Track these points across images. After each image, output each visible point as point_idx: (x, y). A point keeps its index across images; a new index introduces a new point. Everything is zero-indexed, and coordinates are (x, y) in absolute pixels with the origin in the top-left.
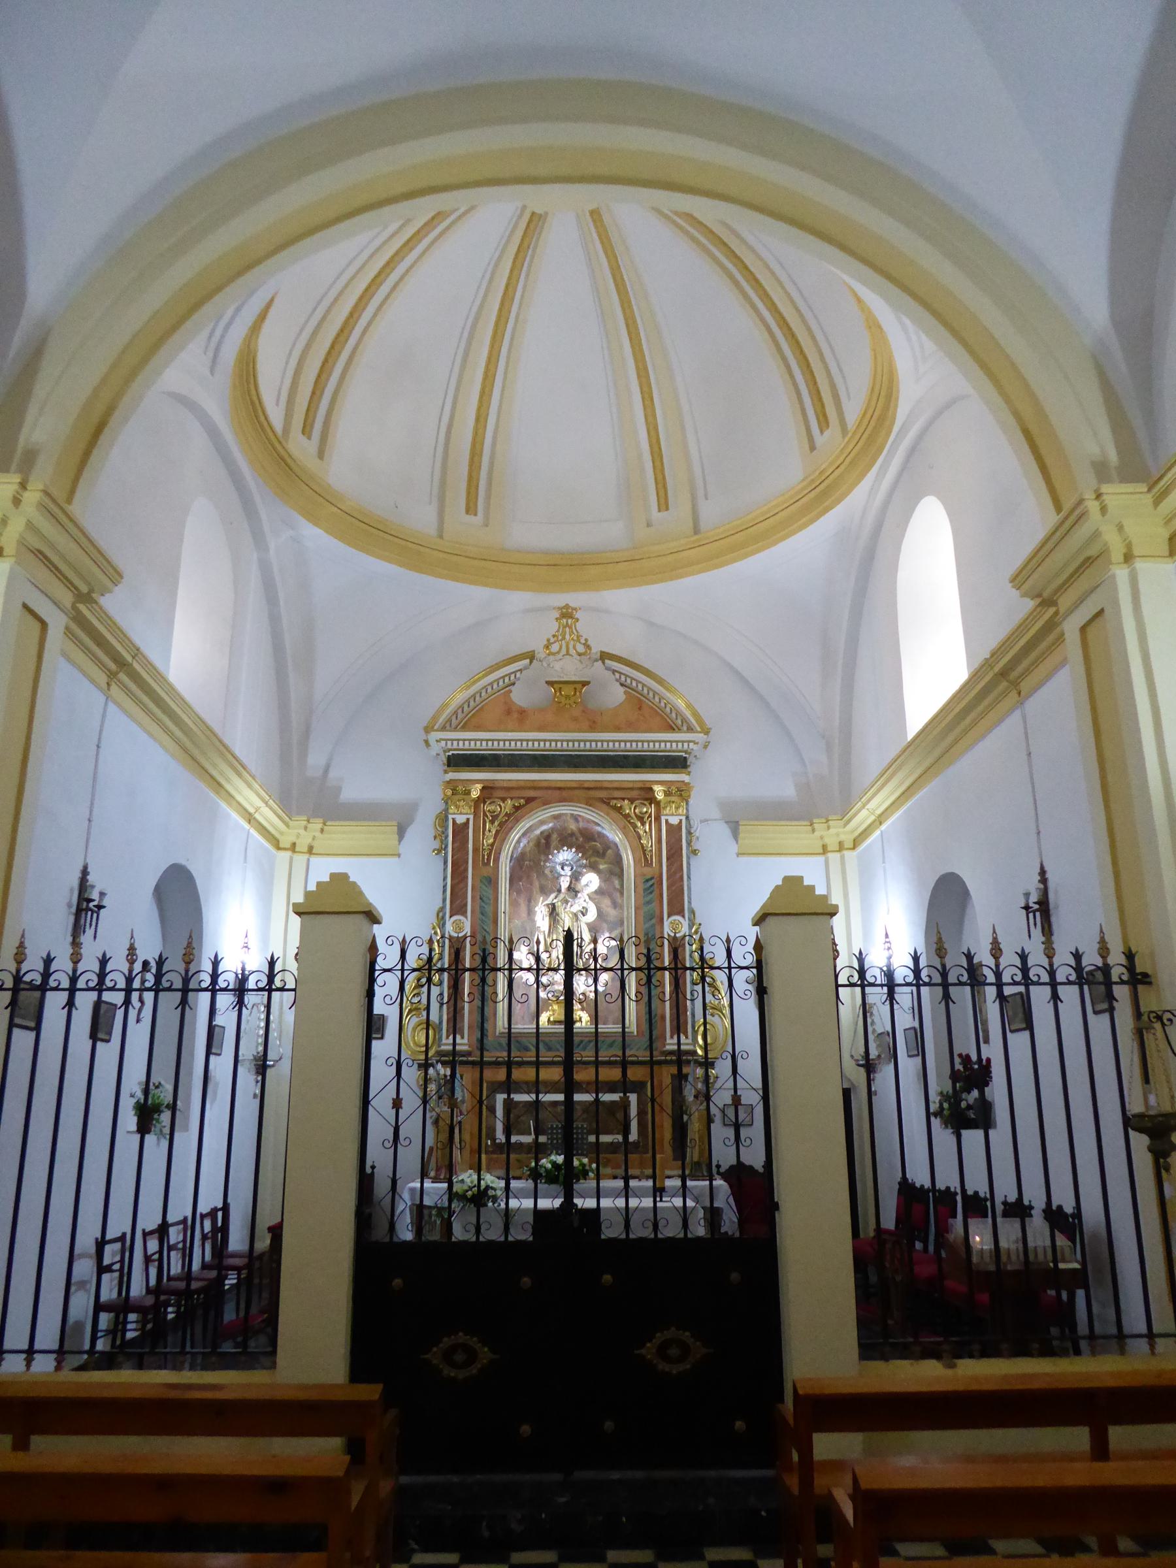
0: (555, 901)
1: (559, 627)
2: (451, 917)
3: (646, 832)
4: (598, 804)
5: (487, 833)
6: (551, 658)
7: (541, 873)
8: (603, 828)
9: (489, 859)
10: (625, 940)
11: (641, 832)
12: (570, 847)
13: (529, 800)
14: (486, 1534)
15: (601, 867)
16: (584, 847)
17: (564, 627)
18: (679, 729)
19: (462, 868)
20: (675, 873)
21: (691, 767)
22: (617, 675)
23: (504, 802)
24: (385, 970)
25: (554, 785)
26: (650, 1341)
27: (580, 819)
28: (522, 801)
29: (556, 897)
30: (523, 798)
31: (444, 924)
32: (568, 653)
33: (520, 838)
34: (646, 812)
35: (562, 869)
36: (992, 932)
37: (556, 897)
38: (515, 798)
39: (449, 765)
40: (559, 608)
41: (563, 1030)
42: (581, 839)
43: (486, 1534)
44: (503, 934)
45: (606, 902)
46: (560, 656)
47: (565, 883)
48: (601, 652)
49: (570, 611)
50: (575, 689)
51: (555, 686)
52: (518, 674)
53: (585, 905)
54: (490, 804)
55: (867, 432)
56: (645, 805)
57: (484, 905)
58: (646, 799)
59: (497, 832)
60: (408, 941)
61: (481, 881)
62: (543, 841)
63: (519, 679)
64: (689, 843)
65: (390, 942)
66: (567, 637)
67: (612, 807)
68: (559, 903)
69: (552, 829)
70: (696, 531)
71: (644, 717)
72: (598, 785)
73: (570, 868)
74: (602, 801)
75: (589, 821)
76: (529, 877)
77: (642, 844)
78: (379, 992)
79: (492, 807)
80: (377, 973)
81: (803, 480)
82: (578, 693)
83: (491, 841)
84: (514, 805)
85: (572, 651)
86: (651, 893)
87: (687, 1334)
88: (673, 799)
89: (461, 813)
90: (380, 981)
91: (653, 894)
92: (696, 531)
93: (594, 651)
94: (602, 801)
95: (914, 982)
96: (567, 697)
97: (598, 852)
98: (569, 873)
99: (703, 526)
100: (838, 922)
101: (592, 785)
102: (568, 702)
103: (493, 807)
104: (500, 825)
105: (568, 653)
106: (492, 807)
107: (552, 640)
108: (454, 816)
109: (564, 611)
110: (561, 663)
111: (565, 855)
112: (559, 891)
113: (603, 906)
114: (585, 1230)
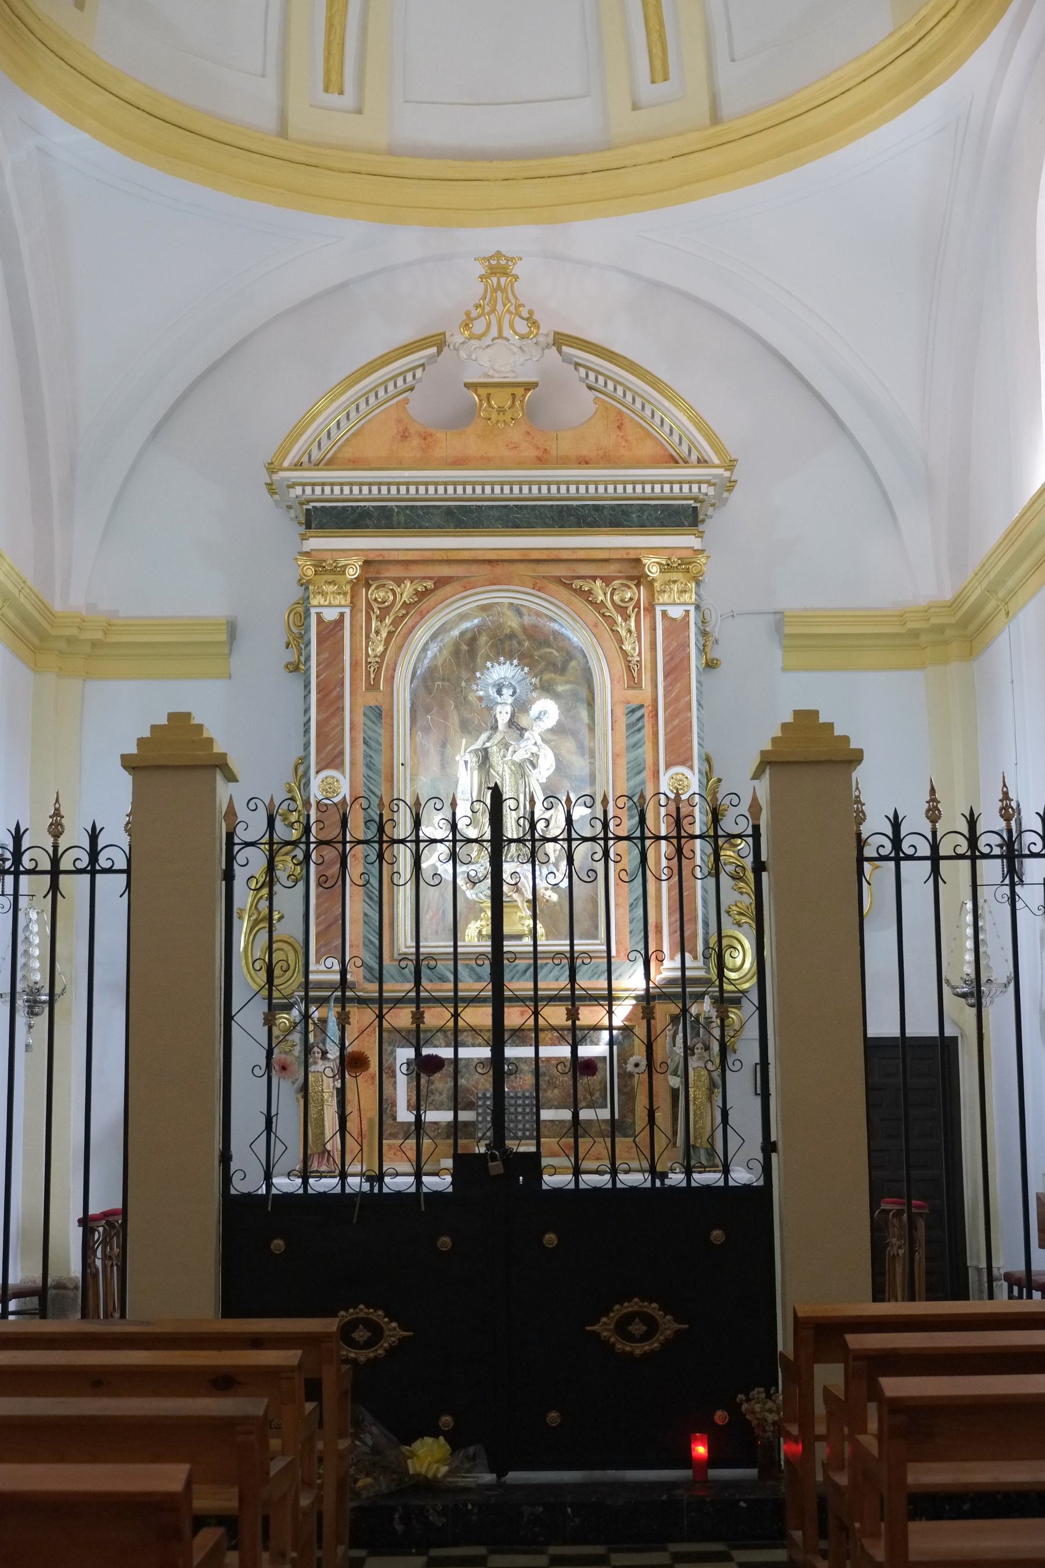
0: (488, 745)
1: (486, 291)
2: (317, 772)
3: (630, 631)
4: (554, 588)
5: (373, 635)
6: (474, 343)
7: (463, 701)
8: (562, 626)
9: (377, 679)
10: (574, 801)
11: (623, 633)
12: (510, 656)
13: (441, 582)
14: (399, 1527)
15: (560, 688)
16: (531, 657)
17: (495, 291)
18: (686, 462)
19: (334, 694)
20: (677, 699)
21: (708, 521)
22: (582, 372)
23: (399, 586)
24: (248, 844)
25: (482, 556)
26: (607, 1315)
27: (523, 610)
28: (430, 584)
29: (489, 739)
30: (431, 578)
31: (307, 784)
32: (500, 336)
33: (427, 643)
34: (631, 599)
35: (499, 692)
36: (1002, 784)
37: (489, 739)
38: (417, 578)
39: (308, 526)
40: (484, 258)
41: (505, 943)
42: (527, 644)
43: (399, 1527)
44: (404, 791)
45: (568, 746)
46: (487, 340)
47: (503, 716)
48: (556, 333)
49: (503, 262)
50: (513, 395)
51: (480, 390)
52: (419, 372)
53: (535, 749)
54: (377, 588)
55: (659, 437)
56: (629, 587)
57: (371, 753)
58: (631, 578)
59: (390, 634)
60: (277, 803)
61: (365, 714)
62: (465, 648)
63: (420, 380)
64: (702, 650)
65: (252, 806)
66: (499, 306)
67: (575, 590)
68: (495, 748)
69: (480, 629)
70: (716, 118)
71: (626, 441)
72: (553, 555)
73: (511, 691)
74: (559, 580)
75: (538, 614)
76: (442, 706)
77: (625, 653)
78: (240, 875)
79: (381, 594)
80: (236, 848)
81: (892, 34)
82: (517, 403)
83: (381, 649)
84: (416, 590)
85: (507, 332)
86: (639, 730)
87: (654, 1305)
88: (674, 576)
89: (330, 606)
90: (240, 858)
91: (643, 732)
92: (716, 118)
93: (543, 330)
94: (559, 580)
95: (969, 853)
96: (501, 410)
97: (554, 665)
98: (510, 700)
99: (727, 108)
100: (860, 774)
101: (543, 556)
102: (501, 417)
103: (382, 594)
104: (395, 623)
105: (500, 336)
106: (381, 594)
107: (474, 314)
108: (318, 610)
109: (493, 262)
110: (489, 351)
111: (503, 671)
112: (495, 728)
113: (563, 752)
114: (521, 1178)
